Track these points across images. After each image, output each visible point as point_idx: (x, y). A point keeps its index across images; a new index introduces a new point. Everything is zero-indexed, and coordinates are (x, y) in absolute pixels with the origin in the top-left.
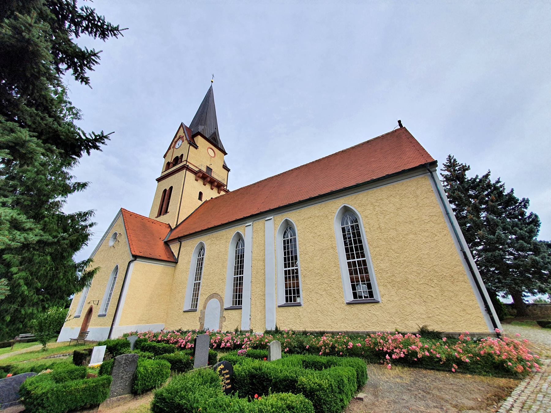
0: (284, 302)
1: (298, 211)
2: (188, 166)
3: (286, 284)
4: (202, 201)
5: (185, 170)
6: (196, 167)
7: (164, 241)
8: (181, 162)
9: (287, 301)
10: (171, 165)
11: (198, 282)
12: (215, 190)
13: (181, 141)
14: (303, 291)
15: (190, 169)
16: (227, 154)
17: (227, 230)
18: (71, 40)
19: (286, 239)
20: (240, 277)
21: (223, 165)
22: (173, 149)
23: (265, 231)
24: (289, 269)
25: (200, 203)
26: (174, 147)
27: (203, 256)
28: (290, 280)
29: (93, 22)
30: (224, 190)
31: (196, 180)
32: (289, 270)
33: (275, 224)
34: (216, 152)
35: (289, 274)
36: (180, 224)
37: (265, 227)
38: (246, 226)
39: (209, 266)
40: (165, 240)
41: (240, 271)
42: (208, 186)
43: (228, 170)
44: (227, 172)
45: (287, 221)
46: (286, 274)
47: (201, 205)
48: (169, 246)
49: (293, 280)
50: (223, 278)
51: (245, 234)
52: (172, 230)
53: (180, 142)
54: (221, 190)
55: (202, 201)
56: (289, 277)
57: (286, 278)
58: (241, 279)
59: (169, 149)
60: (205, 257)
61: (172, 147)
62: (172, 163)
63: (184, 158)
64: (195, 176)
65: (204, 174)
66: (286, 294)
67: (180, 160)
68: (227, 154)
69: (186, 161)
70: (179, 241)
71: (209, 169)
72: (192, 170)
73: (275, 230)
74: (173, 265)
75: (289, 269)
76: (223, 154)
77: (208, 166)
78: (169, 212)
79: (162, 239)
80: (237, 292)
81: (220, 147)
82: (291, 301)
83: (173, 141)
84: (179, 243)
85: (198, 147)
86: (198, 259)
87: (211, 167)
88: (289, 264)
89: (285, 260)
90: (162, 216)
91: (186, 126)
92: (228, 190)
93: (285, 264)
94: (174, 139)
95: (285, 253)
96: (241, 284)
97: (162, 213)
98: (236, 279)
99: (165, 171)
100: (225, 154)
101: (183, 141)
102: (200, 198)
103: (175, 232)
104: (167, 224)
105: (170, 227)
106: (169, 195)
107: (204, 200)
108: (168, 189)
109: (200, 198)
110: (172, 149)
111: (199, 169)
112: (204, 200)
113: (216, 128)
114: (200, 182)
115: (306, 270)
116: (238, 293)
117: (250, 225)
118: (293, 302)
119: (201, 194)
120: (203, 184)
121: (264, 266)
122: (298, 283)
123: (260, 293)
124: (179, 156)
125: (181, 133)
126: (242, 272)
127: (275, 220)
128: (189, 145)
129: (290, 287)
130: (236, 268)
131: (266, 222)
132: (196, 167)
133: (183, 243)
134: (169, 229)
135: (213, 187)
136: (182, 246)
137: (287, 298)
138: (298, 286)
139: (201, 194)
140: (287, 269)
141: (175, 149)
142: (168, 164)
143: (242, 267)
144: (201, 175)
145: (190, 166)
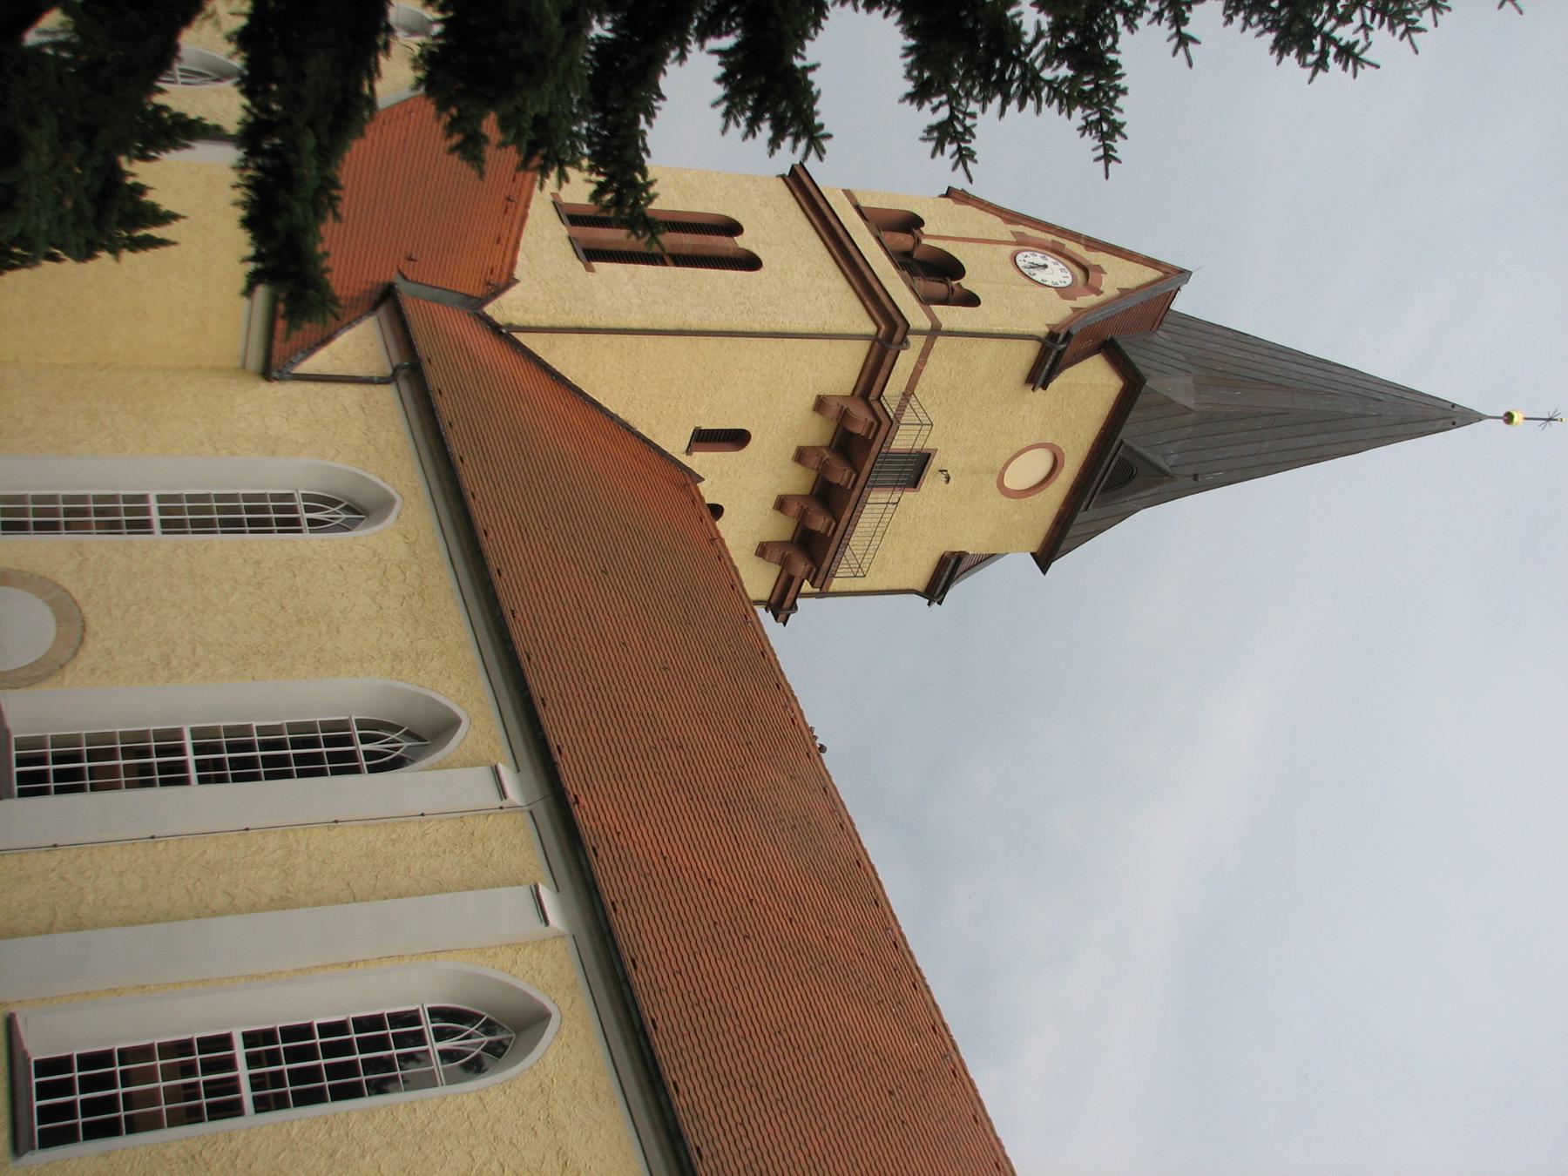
0: (38, 1048)
1: (608, 1082)
2: (904, 343)
3: (144, 1052)
4: (689, 451)
5: (870, 328)
6: (908, 394)
7: (398, 280)
8: (926, 301)
9: (45, 1067)
10: (903, 241)
11: (155, 517)
12: (780, 528)
13: (1069, 281)
14: (106, 1155)
15: (888, 361)
16: (1044, 568)
17: (472, 654)
18: (425, 59)
19: (428, 1026)
20: (182, 767)
21: (959, 557)
22: (1012, 239)
23: (470, 888)
24: (241, 1061)
25: (674, 442)
26: (1022, 242)
27: (311, 522)
28: (168, 1073)
29: (616, 153)
30: (790, 579)
31: (821, 404)
32: (230, 1064)
33: (516, 946)
34: (1037, 499)
35: (208, 1067)
36: (517, 346)
37: (495, 885)
38: (496, 772)
39: (249, 570)
40: (403, 287)
41: (219, 764)
42: (796, 481)
43: (935, 590)
44: (921, 586)
45: (532, 1021)
46: (208, 1044)
47: (662, 453)
48: (374, 308)
49: (172, 1095)
50: (175, 663)
51: (449, 766)
52: (474, 305)
53: (1058, 273)
54: (785, 563)
55: (689, 451)
56: (188, 1070)
57: (183, 1047)
58: (174, 775)
59: (1010, 217)
60: (307, 541)
61: (1020, 228)
62: (919, 241)
63: (951, 316)
64: (848, 391)
65: (867, 443)
66: (87, 1061)
67: (938, 288)
68: (1044, 568)
69: (935, 331)
70: (395, 370)
71: (913, 469)
72: (883, 372)
73: (481, 950)
74: (255, 358)
75: (241, 1061)
76: (1036, 540)
77: (935, 463)
78: (590, 269)
79: (407, 267)
80: (92, 756)
81: (1081, 517)
82: (44, 1091)
83: (1063, 232)
84: (389, 371)
85: (1045, 387)
86: (290, 497)
87: (930, 481)
88: (273, 1058)
89: (290, 1033)
90: (563, 231)
91: (1171, 296)
92: (794, 607)
93: (267, 1036)
94: (1075, 237)
95: (339, 1027)
96: (142, 778)
97: (580, 231)
98: (170, 744)
99: (858, 208)
100: (1044, 558)
101: (1064, 292)
102: (705, 438)
103: (460, 325)
104: (510, 274)
105: (496, 291)
106: (705, 252)
107: (699, 461)
108: (743, 242)
109: (705, 438)
110: (1003, 230)
111: (901, 408)
112: (699, 461)
113: (1198, 484)
114: (816, 432)
115: (233, 1165)
116: (86, 765)
117: (503, 794)
118: (36, 1104)
119: (737, 439)
120: (805, 443)
121: (253, 908)
122: (153, 1123)
123: (90, 898)
124: (966, 283)
125: (1119, 277)
126: (211, 773)
127: (540, 943)
128: (1041, 329)
129: (127, 1079)
130: (239, 740)
131: (523, 893)
132: (908, 394)
133: (387, 394)
134: (478, 291)
135: (794, 508)
136: (365, 389)
137: (63, 1064)
138: (134, 1126)
139: (737, 439)
140: (240, 1052)
141: (1009, 250)
142: (912, 223)
143: (245, 772)
144: (859, 429)
145: (905, 361)
